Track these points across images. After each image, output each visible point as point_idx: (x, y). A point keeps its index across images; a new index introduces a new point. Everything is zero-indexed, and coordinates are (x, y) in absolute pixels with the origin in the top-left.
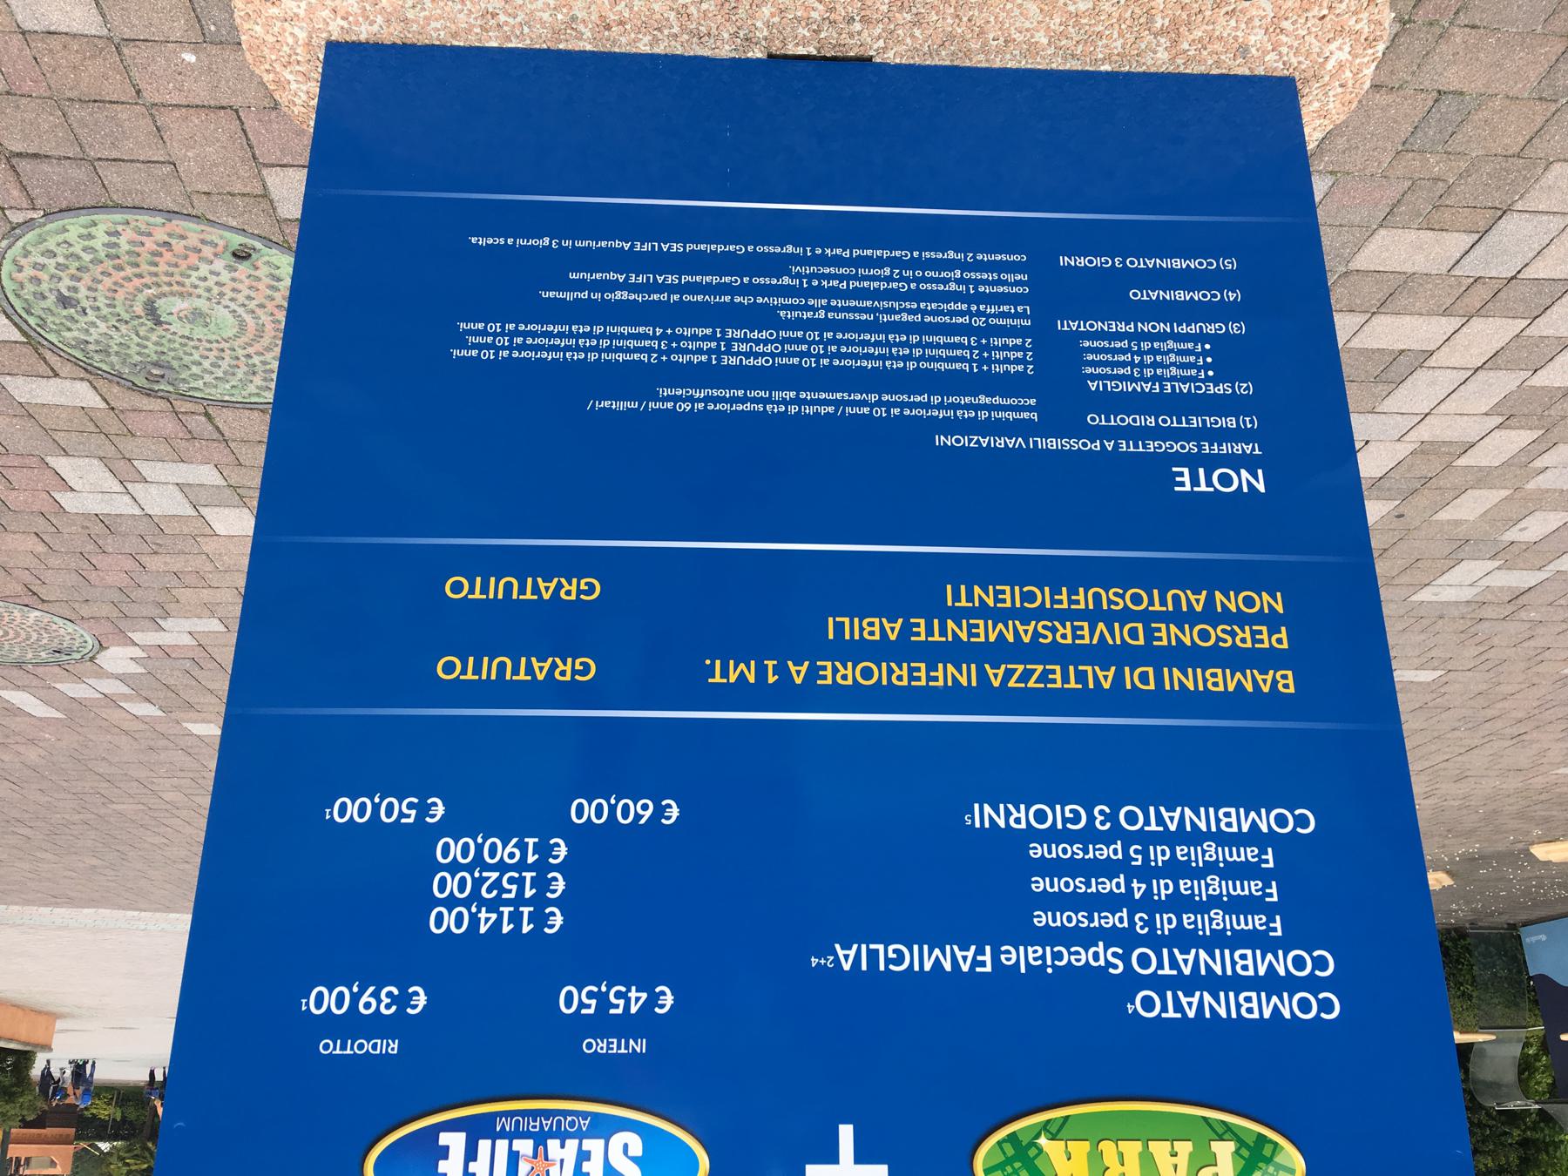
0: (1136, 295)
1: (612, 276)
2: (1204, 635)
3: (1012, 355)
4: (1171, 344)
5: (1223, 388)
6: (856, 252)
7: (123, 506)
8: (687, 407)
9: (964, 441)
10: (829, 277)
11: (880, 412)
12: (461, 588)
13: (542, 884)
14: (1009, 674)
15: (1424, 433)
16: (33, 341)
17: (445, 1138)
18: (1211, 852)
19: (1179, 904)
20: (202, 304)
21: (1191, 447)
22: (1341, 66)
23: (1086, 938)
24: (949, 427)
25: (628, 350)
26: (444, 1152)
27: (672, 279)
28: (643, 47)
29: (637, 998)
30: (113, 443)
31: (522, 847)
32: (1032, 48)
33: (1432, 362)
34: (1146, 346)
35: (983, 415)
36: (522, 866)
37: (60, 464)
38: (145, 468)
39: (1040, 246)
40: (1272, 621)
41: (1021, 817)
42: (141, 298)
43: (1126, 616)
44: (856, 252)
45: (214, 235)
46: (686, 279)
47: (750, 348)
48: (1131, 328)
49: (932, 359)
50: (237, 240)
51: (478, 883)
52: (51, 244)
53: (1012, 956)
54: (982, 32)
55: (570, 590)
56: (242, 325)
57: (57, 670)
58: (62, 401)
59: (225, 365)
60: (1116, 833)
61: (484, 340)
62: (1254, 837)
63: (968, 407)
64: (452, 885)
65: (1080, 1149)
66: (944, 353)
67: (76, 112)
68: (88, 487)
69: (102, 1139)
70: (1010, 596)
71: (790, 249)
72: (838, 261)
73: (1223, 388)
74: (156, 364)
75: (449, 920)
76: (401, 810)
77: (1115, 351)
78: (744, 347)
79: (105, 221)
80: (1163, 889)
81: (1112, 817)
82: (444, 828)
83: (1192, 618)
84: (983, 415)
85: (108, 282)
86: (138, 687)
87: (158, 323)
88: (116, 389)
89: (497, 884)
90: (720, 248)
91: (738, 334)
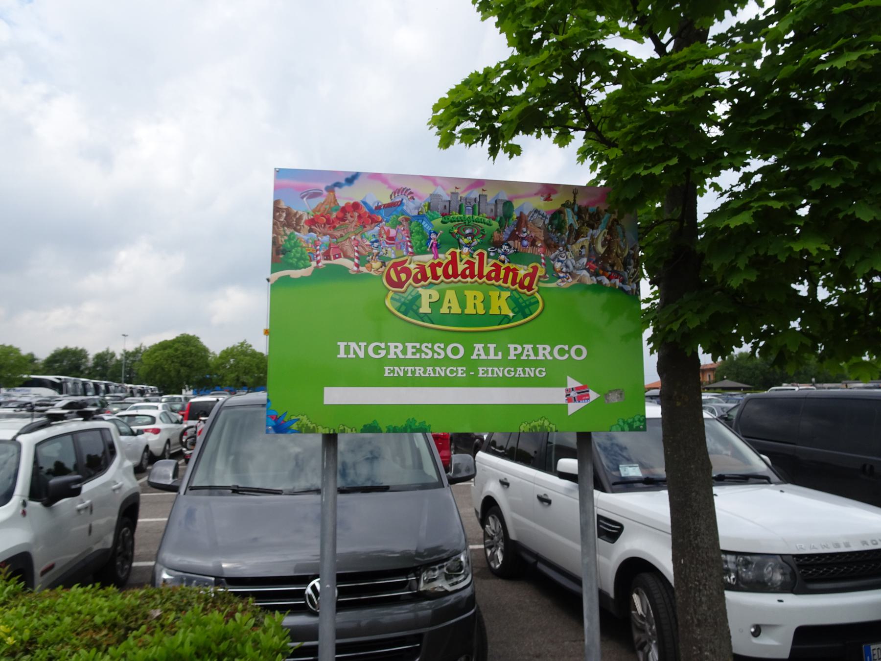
65: (494, 311)
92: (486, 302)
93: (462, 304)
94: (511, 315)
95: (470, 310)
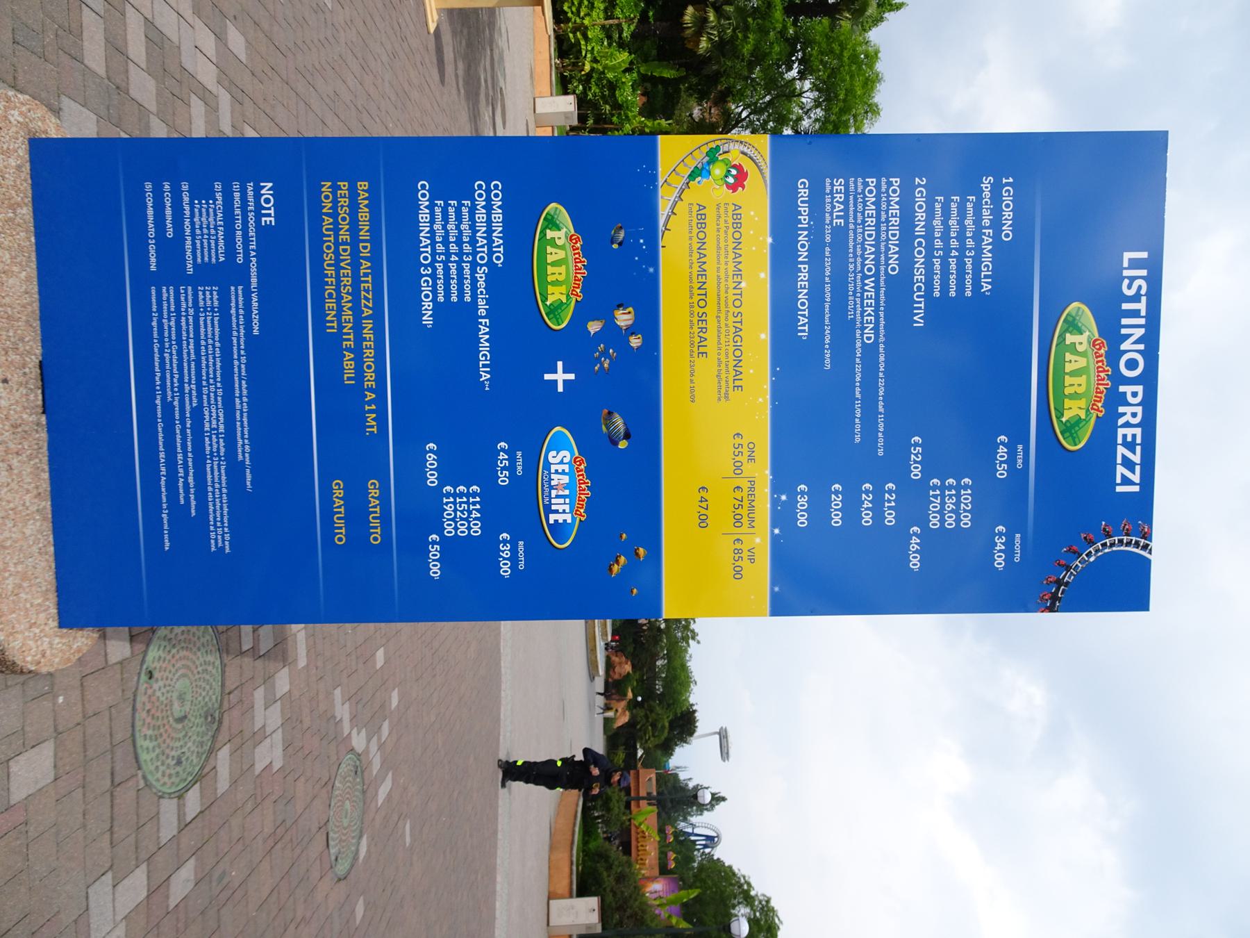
0: (170, 234)
1: (181, 484)
2: (344, 219)
3: (208, 296)
4: (196, 219)
5: (219, 196)
6: (157, 369)
7: (278, 736)
8: (247, 447)
9: (256, 321)
10: (172, 383)
11: (244, 360)
12: (340, 537)
13: (461, 495)
14: (366, 306)
15: (188, 14)
16: (199, 778)
17: (551, 522)
18: (438, 226)
19: (459, 242)
20: (175, 695)
21: (251, 215)
22: (21, 113)
23: (474, 281)
24: (249, 327)
25: (220, 475)
26: (556, 521)
27: (180, 457)
28: (46, 476)
29: (502, 456)
30: (249, 740)
31: (447, 503)
32: (28, 279)
33: (149, 17)
34: (198, 232)
35: (241, 312)
36: (455, 503)
37: (259, 767)
38: (258, 726)
39: (143, 280)
40: (335, 188)
41: (427, 304)
42: (175, 725)
43: (336, 253)
44: (157, 369)
45: (143, 687)
46: (179, 450)
47: (214, 419)
48: (189, 238)
49: (213, 334)
50: (144, 677)
51: (462, 519)
52: (152, 768)
53: (482, 312)
54: (24, 306)
55: (338, 493)
56: (184, 676)
57: (366, 774)
58: (227, 765)
59: (204, 685)
60: (432, 265)
61: (220, 538)
62: (431, 207)
63: (238, 319)
64: (463, 528)
65: (550, 289)
66: (210, 329)
67: (90, 753)
68: (270, 754)
69: (636, 754)
70: (330, 304)
71: (158, 402)
72: (163, 378)
73: (219, 196)
74: (206, 718)
75: (476, 528)
76: (434, 551)
77: (202, 247)
78: (214, 422)
79: (140, 742)
80: (454, 248)
81: (426, 266)
82: (440, 533)
83: (336, 223)
84: (241, 312)
85: (168, 741)
86: (374, 732)
87: (185, 717)
88: (220, 738)
89: (462, 512)
90: (161, 435)
91: (207, 425)
92: (557, 283)
93: (1074, 373)
94: (1064, 420)
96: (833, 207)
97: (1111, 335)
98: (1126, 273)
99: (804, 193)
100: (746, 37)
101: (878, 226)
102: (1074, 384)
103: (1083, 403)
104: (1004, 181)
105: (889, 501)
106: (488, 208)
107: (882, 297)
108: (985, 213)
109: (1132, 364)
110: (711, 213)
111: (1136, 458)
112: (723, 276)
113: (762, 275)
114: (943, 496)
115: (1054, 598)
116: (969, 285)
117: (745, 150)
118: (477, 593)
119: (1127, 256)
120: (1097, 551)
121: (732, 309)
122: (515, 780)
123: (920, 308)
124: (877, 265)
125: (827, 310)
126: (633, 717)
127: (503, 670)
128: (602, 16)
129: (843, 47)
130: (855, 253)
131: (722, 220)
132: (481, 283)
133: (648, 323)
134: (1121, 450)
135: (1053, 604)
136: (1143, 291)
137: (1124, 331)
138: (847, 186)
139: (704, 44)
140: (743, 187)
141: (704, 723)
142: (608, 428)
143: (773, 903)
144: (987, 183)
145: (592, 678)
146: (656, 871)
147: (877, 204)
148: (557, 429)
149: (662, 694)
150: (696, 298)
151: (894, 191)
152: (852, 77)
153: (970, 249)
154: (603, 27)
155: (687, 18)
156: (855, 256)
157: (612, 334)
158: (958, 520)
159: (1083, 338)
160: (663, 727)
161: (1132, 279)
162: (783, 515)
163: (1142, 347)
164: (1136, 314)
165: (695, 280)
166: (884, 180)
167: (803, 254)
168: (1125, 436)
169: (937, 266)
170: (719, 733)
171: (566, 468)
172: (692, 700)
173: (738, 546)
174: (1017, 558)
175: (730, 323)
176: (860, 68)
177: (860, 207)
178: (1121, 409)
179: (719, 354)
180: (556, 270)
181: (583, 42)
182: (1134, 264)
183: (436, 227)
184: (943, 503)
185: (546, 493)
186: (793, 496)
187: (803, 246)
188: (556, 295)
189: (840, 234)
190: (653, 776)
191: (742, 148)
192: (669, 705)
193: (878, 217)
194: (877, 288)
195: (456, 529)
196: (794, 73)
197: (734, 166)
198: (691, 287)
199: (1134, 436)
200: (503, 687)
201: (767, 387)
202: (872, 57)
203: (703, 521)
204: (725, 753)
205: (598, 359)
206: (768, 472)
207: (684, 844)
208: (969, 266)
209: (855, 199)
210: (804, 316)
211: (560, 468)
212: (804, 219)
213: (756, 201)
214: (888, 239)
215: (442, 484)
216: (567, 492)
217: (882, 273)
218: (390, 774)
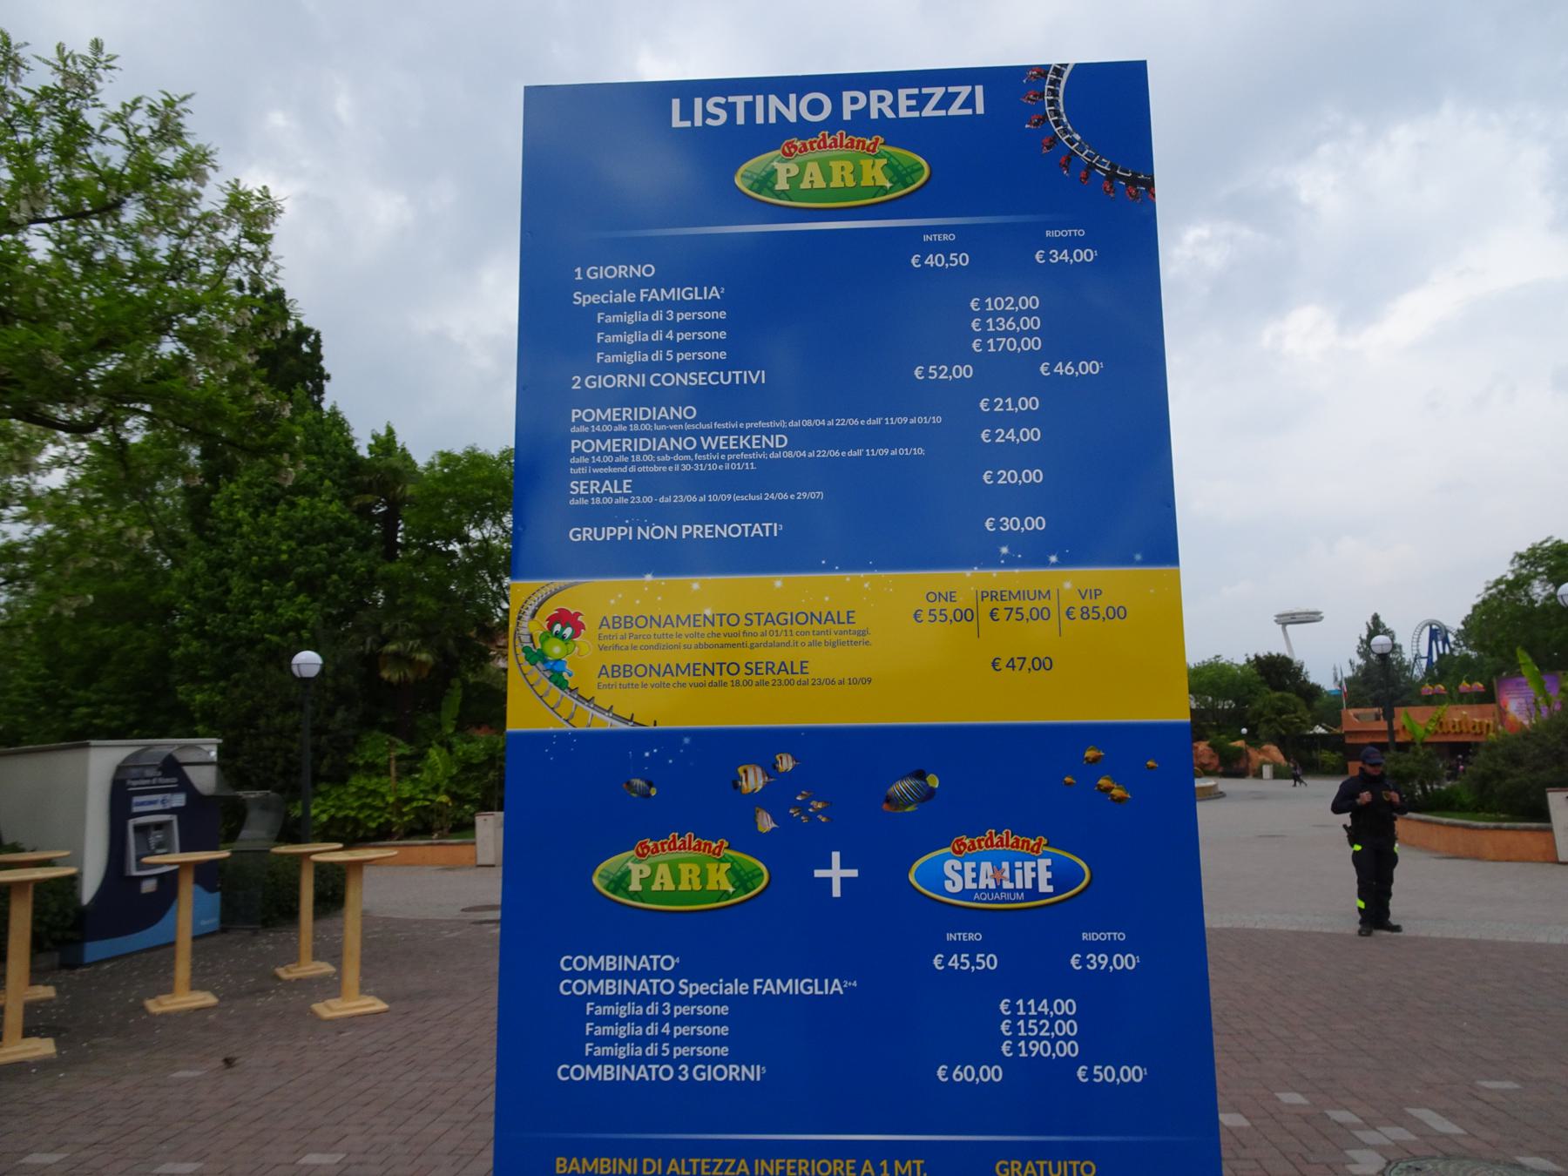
14: (734, 1169)
17: (1050, 889)
18: (621, 1053)
26: (1049, 882)
29: (954, 962)
31: (1029, 1051)
36: (1028, 1039)
41: (732, 1072)
51: (1051, 1029)
53: (742, 989)
60: (676, 1063)
62: (594, 1062)
64: (1066, 1028)
65: (712, 886)
75: (1065, 1007)
76: (1103, 1074)
80: (652, 1029)
81: (678, 1073)
89: (1041, 1028)
92: (704, 877)
95: (684, 886)
96: (607, 494)
97: (778, 135)
98: (698, 122)
99: (588, 534)
100: (419, 606)
101: (632, 435)
102: (842, 175)
103: (866, 163)
104: (579, 278)
105: (1005, 406)
106: (598, 977)
107: (726, 425)
108: (619, 299)
109: (815, 107)
110: (611, 658)
111: (939, 92)
112: (697, 641)
113: (696, 586)
114: (996, 334)
115: (1134, 181)
116: (711, 315)
117: (529, 612)
118: (1165, 1010)
119: (677, 122)
120: (1066, 131)
121: (741, 627)
122: (1388, 913)
123: (741, 376)
124: (684, 434)
125: (743, 498)
126: (1271, 740)
127: (1226, 925)
128: (385, 780)
129: (436, 493)
130: (667, 464)
131: (621, 643)
132: (702, 989)
133: (759, 744)
134: (928, 112)
135: (1142, 183)
136: (722, 100)
137: (772, 120)
138: (580, 477)
139: (424, 657)
140: (578, 614)
141: (1271, 644)
142: (908, 804)
143: (1523, 549)
144: (581, 300)
145: (1221, 795)
146: (1490, 708)
147: (603, 437)
148: (912, 878)
149: (1236, 701)
150: (726, 677)
151: (589, 415)
152: (470, 482)
153: (665, 315)
154: (399, 779)
155: (395, 677)
156: (672, 463)
157: (776, 795)
158: (1030, 313)
159: (781, 168)
160: (1282, 699)
161: (706, 114)
162: (1031, 553)
163: (793, 97)
164: (750, 108)
165: (700, 679)
166: (574, 430)
167: (668, 532)
168: (909, 109)
169: (686, 356)
170: (1284, 624)
171: (969, 865)
172: (1242, 662)
173: (1077, 613)
174: (1080, 233)
175: (761, 629)
176: (460, 472)
177: (608, 459)
178: (874, 115)
179: (803, 644)
180: (685, 877)
181: (415, 804)
182: (687, 113)
183: (623, 1015)
184: (1006, 334)
185: (1008, 896)
186: (1001, 537)
187: (657, 532)
188: (719, 878)
189: (642, 483)
190: (1352, 712)
191: (526, 617)
192: (1250, 692)
193: (621, 435)
194: (714, 433)
195: (1067, 1038)
196: (456, 547)
197: (550, 627)
198: (711, 684)
199: (909, 97)
200: (1250, 925)
201: (849, 576)
202: (447, 458)
203: (1042, 664)
204: (1312, 617)
205: (812, 817)
206: (968, 573)
207: (1443, 669)
208: (686, 316)
209: (598, 465)
210: (751, 529)
211: (969, 875)
212: (621, 532)
213: (595, 596)
214: (651, 421)
215: (998, 1058)
216: (1005, 865)
217: (694, 427)
218: (1410, 1110)
